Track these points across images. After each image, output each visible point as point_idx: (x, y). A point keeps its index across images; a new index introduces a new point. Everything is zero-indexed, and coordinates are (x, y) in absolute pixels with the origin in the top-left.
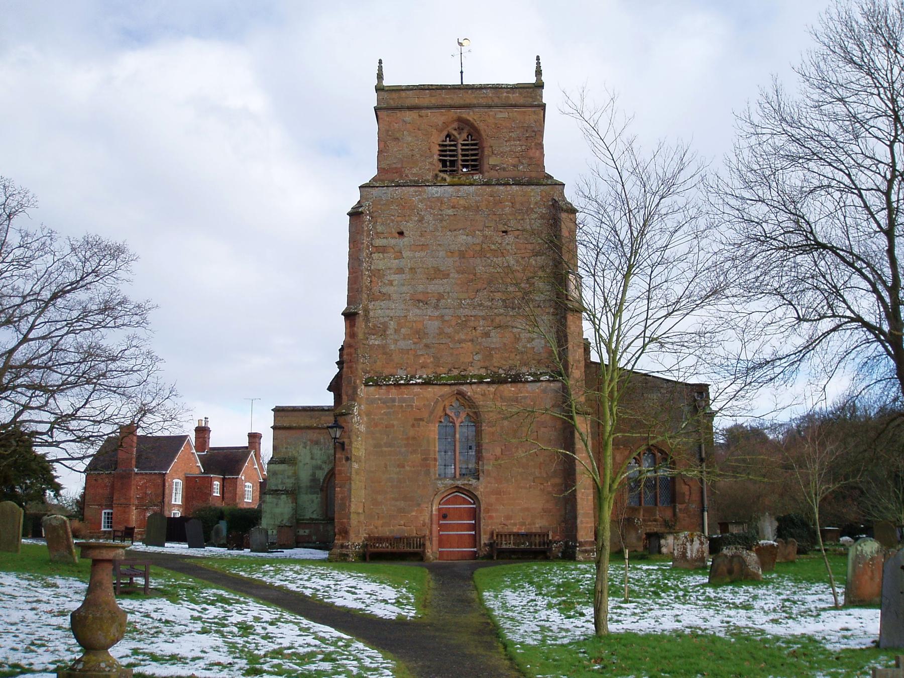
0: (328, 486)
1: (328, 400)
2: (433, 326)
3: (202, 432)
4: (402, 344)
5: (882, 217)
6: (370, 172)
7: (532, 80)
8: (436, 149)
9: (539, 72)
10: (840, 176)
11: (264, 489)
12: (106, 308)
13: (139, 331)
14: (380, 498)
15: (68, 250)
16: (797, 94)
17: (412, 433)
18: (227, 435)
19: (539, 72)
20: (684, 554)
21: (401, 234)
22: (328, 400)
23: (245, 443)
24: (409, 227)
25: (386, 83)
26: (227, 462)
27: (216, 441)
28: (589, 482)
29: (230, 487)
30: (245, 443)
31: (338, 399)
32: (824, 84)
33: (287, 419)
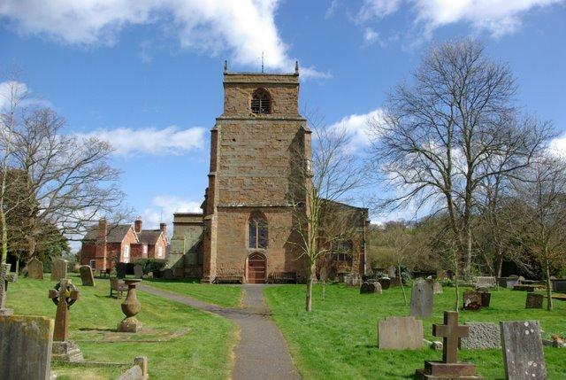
0: (201, 249)
1: (200, 211)
2: (247, 181)
3: (138, 223)
4: (234, 189)
5: (446, 138)
6: (220, 112)
7: (293, 71)
8: (250, 103)
9: (297, 69)
10: (428, 119)
11: (168, 249)
12: (100, 171)
13: (117, 183)
14: (223, 257)
15: (82, 144)
16: (411, 84)
17: (237, 228)
18: (151, 222)
19: (297, 69)
20: (351, 282)
21: (234, 140)
22: (200, 211)
23: (158, 228)
24: (237, 137)
25: (228, 72)
26: (150, 238)
27: (144, 227)
28: (392, 213)
29: (151, 247)
30: (158, 228)
31: (205, 211)
32: (423, 79)
33: (182, 220)
